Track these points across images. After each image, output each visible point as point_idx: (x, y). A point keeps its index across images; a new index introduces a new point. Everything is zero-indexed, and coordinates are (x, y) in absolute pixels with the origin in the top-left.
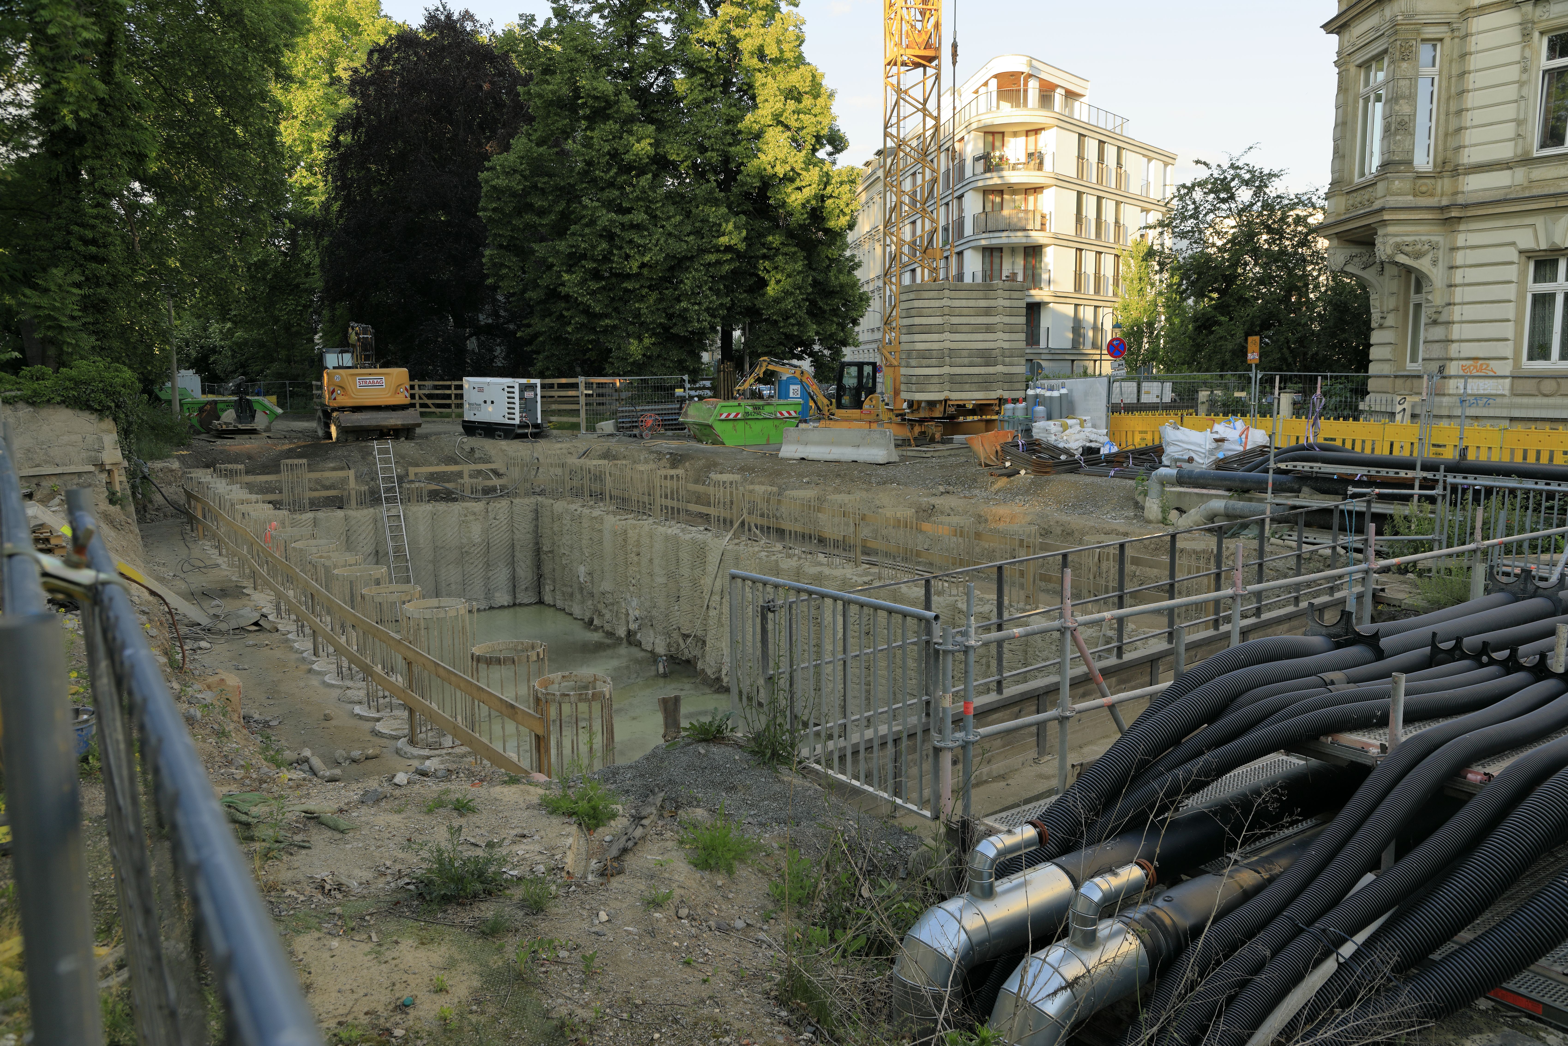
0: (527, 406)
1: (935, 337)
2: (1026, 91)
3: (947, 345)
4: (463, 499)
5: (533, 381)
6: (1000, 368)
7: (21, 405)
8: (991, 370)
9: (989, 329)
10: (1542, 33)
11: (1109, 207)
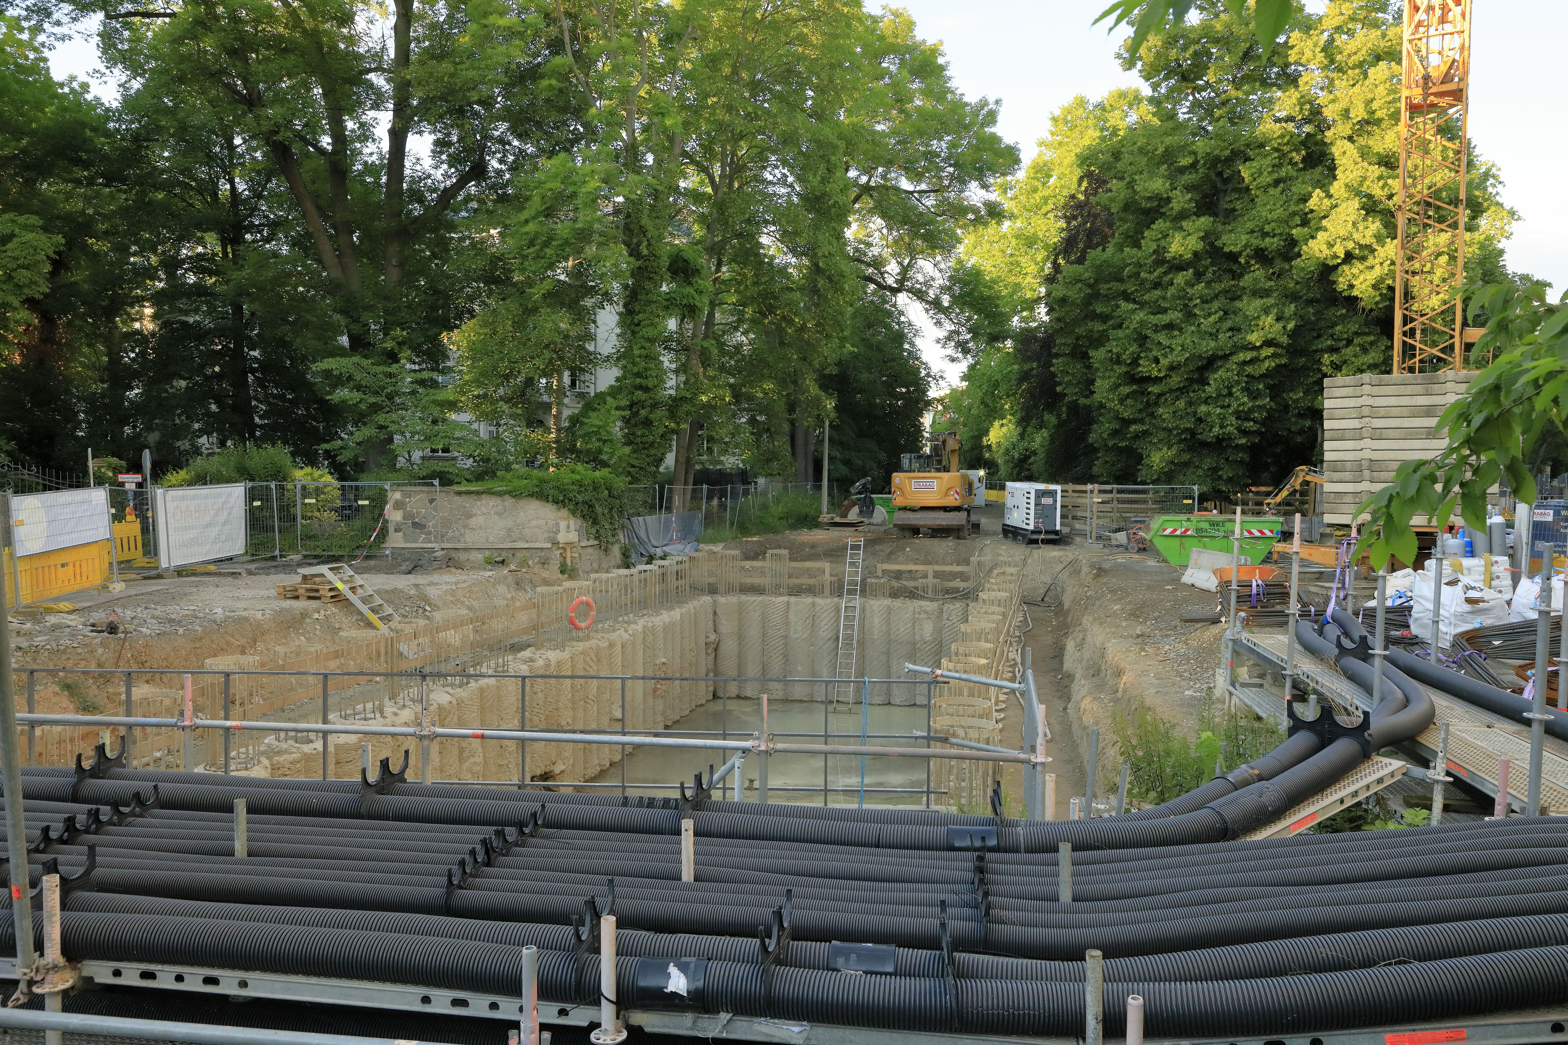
0: (1044, 512)
1: (1349, 444)
3: (1367, 454)
4: (923, 598)
5: (1052, 487)
7: (507, 497)
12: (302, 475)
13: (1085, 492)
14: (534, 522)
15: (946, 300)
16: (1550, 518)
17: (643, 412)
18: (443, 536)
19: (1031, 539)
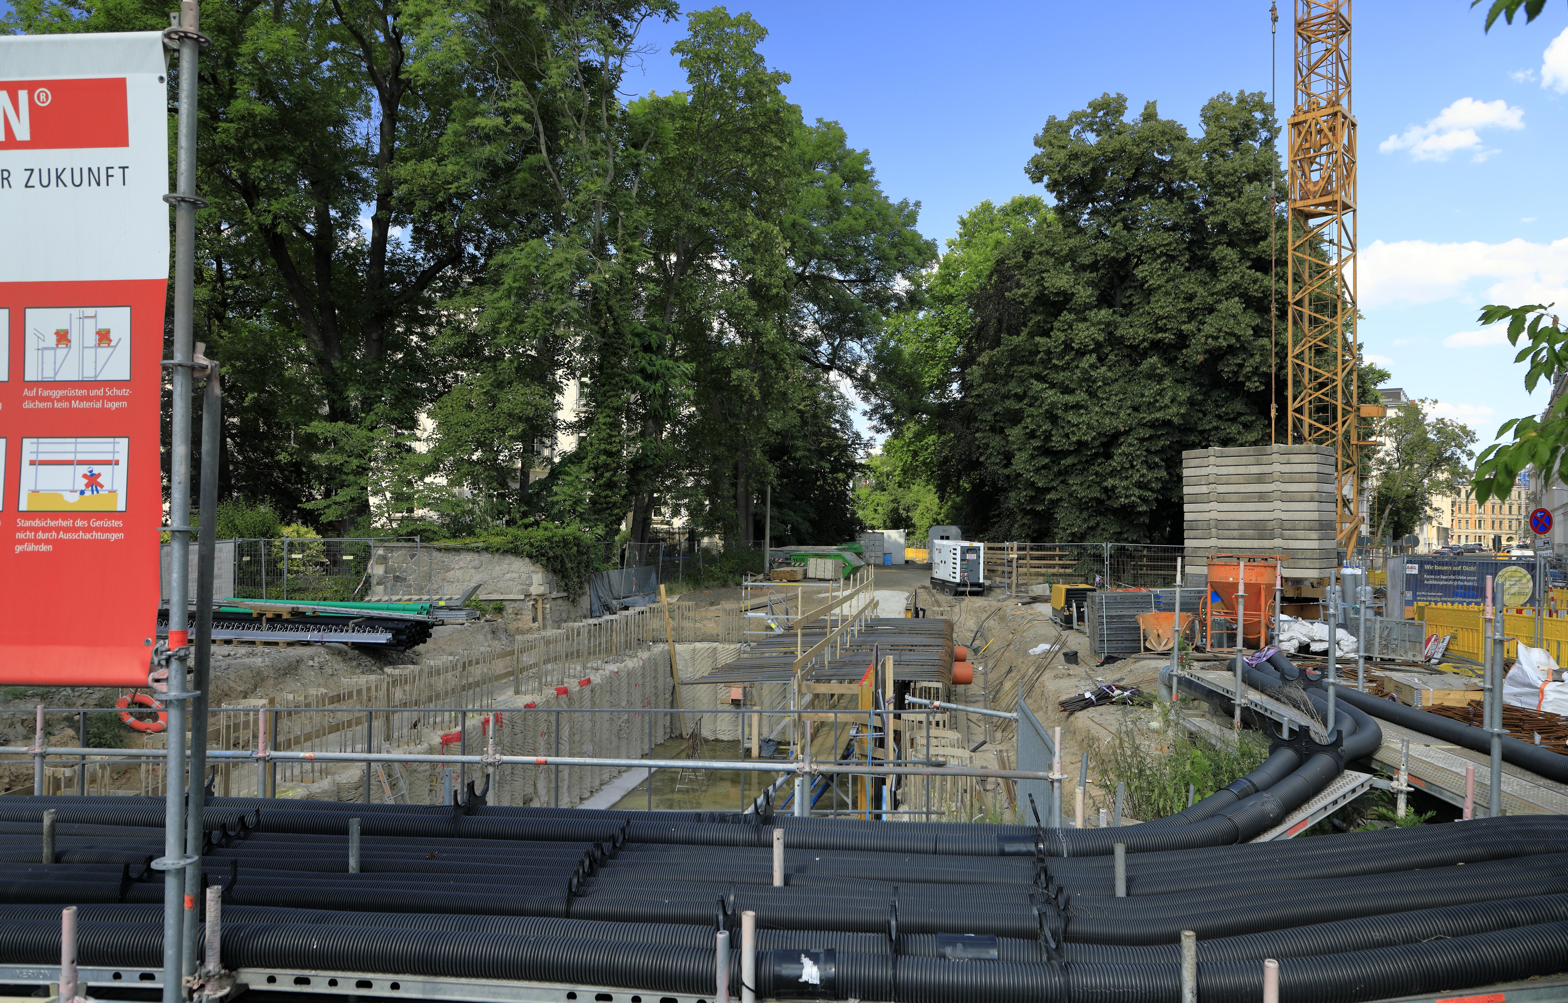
0: (968, 567)
5: (976, 544)
6: (1278, 542)
8: (1267, 544)
9: (1262, 497)
12: (290, 532)
13: (1003, 549)
14: (509, 575)
15: (873, 377)
16: (1416, 572)
17: (607, 475)
18: (422, 589)
19: (958, 591)
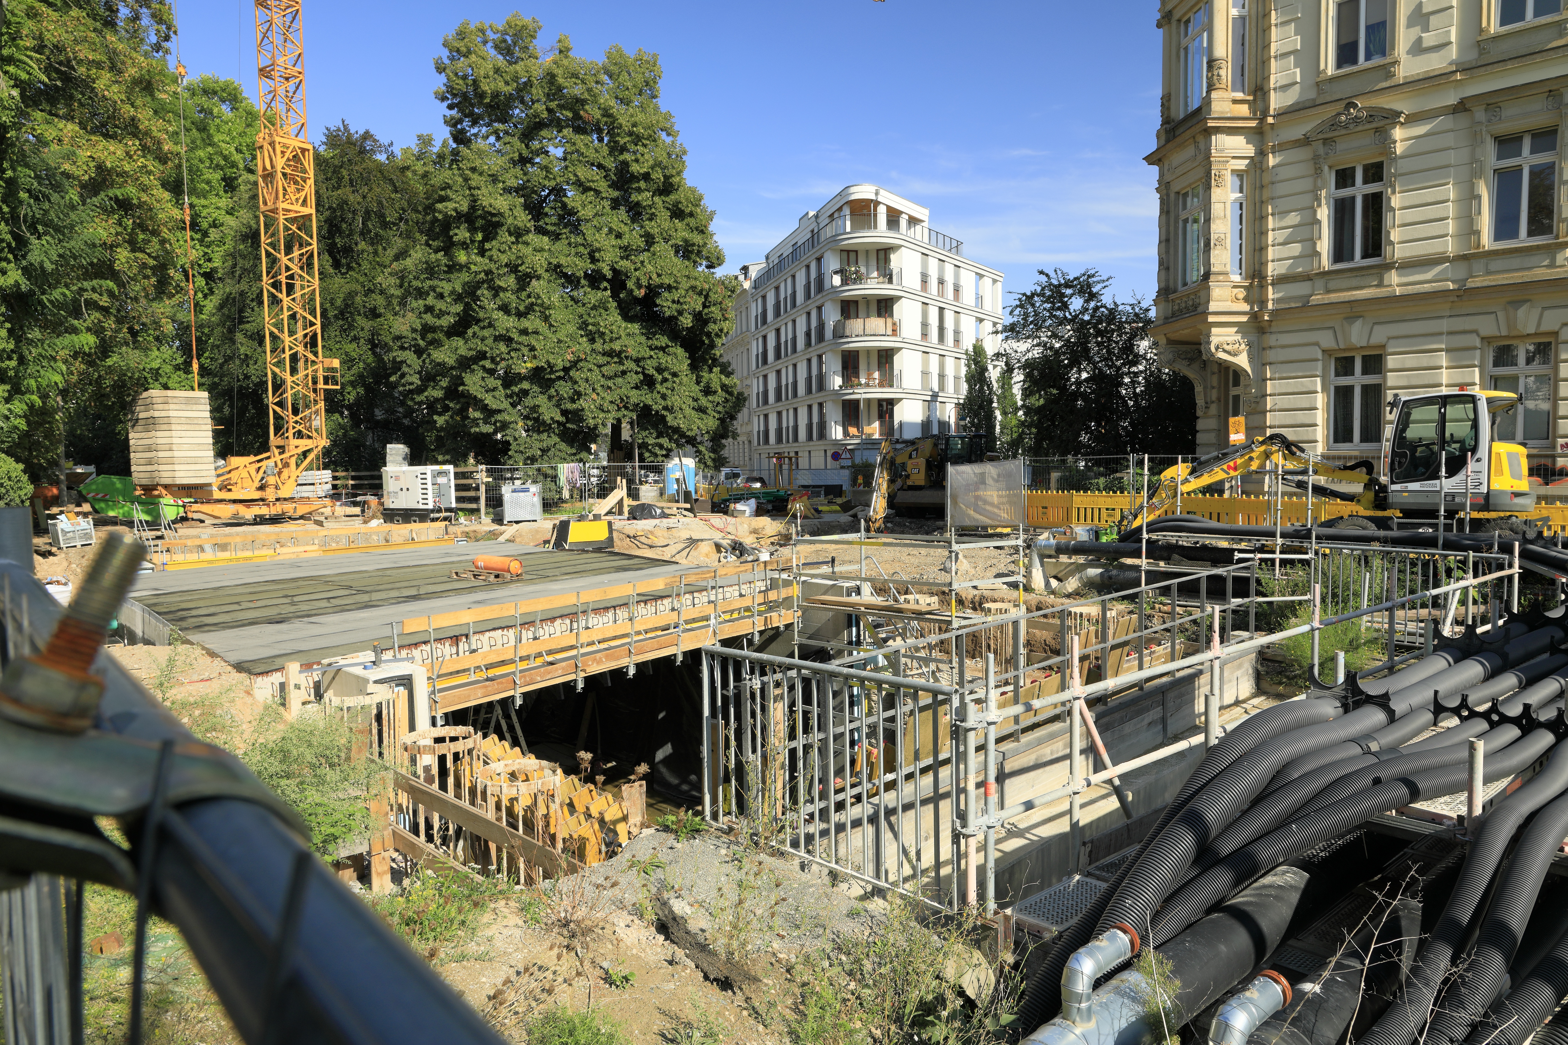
2: (875, 215)
10: (1330, 167)
11: (949, 316)
